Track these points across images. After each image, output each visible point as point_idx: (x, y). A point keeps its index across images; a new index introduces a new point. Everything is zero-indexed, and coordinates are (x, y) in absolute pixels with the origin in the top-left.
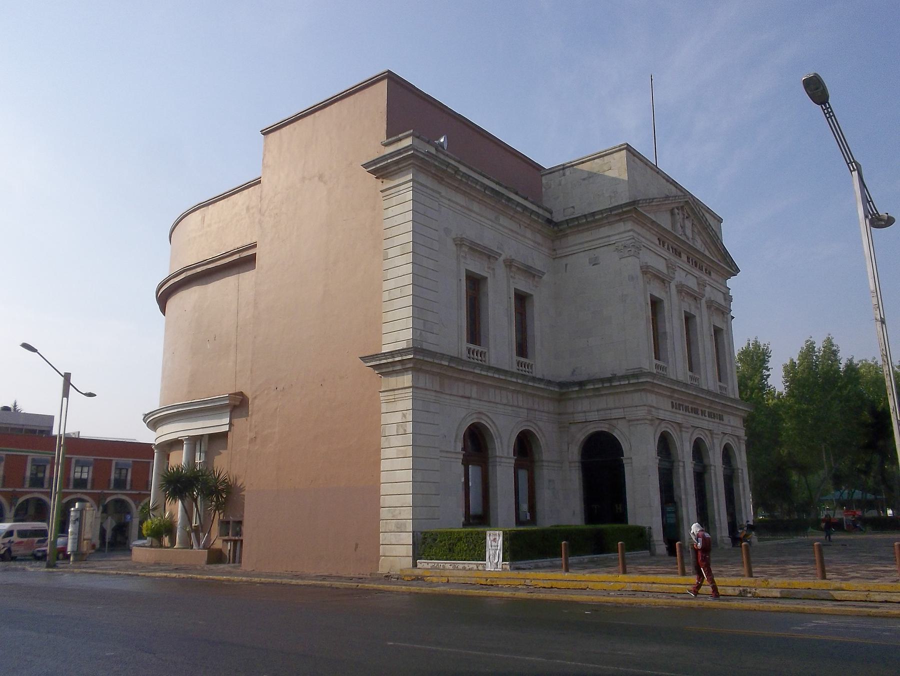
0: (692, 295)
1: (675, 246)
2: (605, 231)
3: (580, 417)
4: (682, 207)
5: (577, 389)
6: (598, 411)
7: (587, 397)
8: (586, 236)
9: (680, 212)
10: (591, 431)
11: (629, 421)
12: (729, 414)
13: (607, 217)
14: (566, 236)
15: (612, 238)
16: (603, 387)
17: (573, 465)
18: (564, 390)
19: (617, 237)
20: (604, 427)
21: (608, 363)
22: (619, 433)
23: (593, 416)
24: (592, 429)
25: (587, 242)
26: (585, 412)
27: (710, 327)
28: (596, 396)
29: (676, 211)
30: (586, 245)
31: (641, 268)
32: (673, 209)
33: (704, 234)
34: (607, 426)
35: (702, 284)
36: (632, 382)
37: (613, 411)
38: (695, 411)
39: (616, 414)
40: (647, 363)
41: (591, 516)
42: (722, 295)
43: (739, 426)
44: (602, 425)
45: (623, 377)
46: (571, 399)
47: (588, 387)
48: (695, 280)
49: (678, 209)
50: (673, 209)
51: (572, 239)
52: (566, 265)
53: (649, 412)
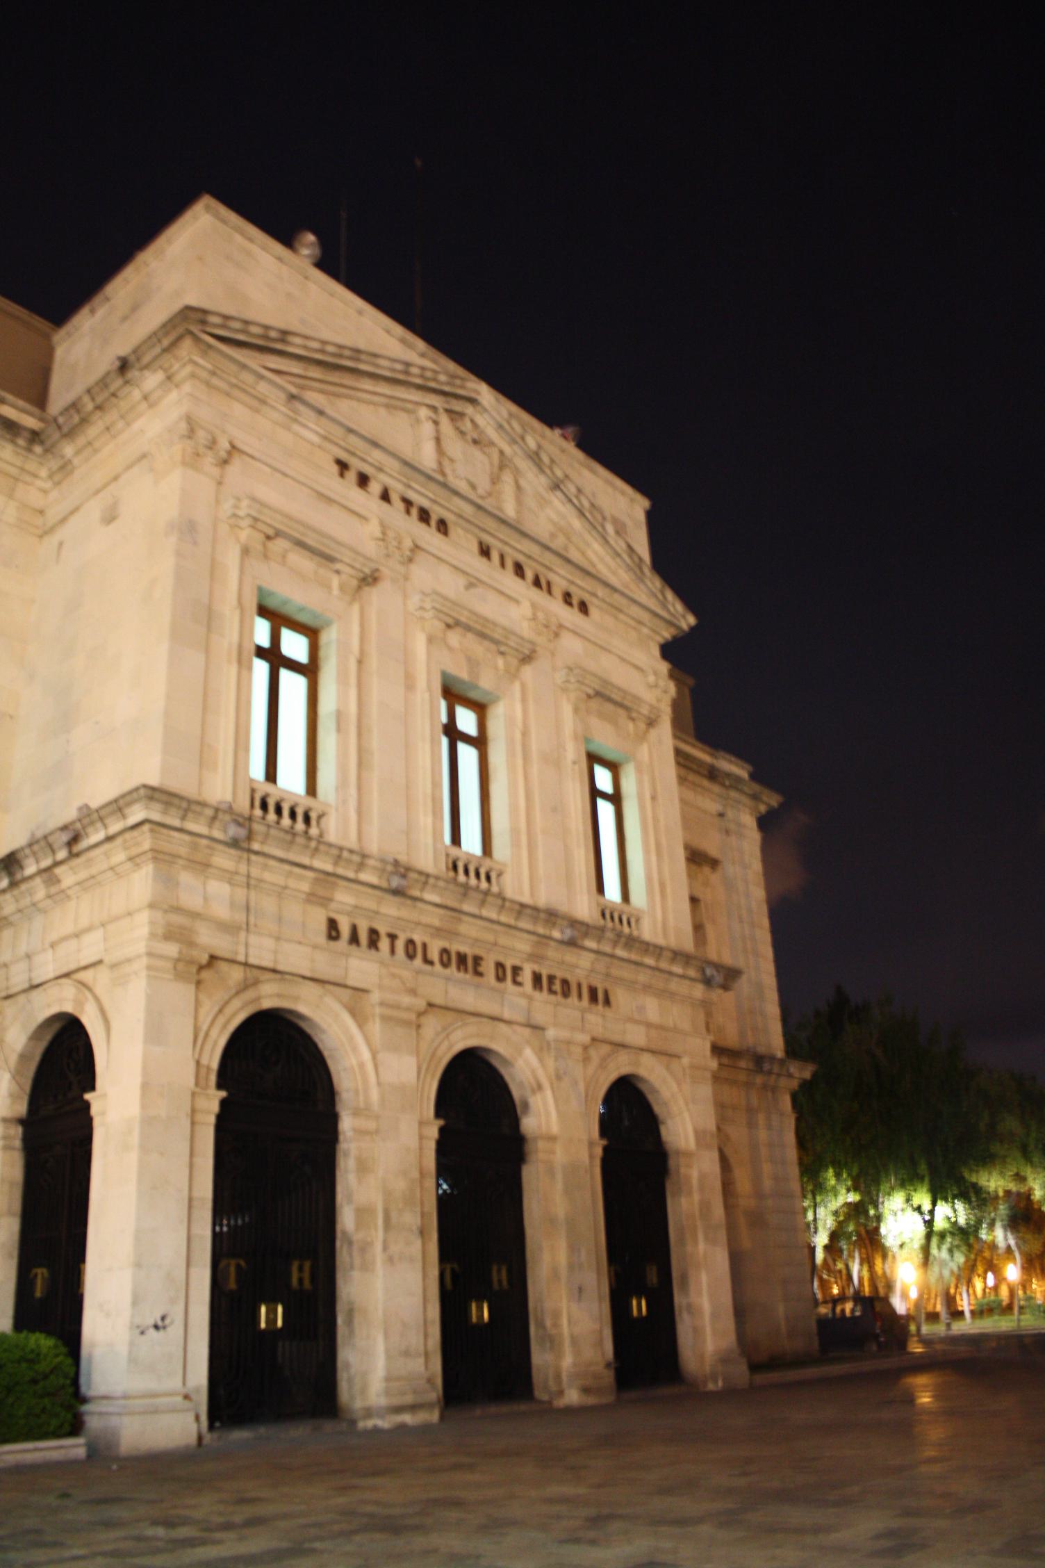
11: (114, 966)
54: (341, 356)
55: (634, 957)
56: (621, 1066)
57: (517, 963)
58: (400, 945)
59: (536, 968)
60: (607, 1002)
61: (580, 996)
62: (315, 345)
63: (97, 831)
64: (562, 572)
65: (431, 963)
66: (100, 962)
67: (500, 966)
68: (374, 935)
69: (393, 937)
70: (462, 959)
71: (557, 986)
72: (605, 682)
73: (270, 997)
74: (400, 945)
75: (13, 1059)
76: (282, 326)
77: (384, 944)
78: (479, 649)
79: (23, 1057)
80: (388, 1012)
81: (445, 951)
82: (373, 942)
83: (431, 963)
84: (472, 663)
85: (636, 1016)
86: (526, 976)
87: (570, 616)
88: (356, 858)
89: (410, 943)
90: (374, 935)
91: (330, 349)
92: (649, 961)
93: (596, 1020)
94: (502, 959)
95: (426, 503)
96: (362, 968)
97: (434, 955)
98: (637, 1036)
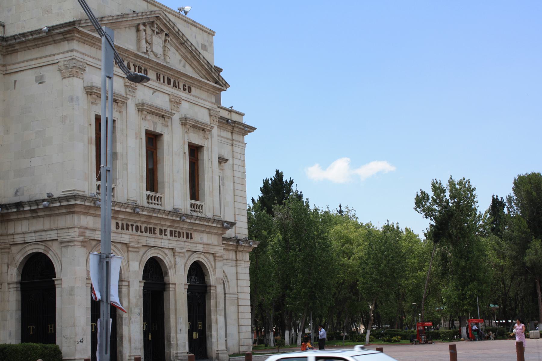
0: (157, 115)
1: (138, 64)
2: (50, 49)
3: (19, 239)
4: (153, 23)
5: (15, 210)
6: (35, 232)
7: (26, 218)
8: (35, 53)
9: (148, 28)
10: (29, 252)
11: (62, 243)
12: (199, 231)
13: (165, 11)
14: (16, 51)
15: (56, 57)
16: (38, 209)
17: (11, 286)
18: (5, 211)
19: (61, 56)
20: (40, 249)
21: (49, 183)
22: (53, 255)
23: (31, 238)
24: (30, 250)
25: (33, 60)
26: (23, 233)
27: (184, 143)
28: (34, 217)
29: (142, 27)
30: (33, 62)
31: (85, 88)
32: (139, 25)
33: (183, 49)
34: (43, 247)
35: (176, 102)
36: (62, 204)
37: (48, 233)
38: (152, 231)
39: (51, 235)
40: (84, 183)
41: (25, 336)
42: (206, 112)
43: (216, 243)
44: (40, 247)
45: (59, 199)
46: (12, 220)
47: (26, 209)
48: (167, 97)
49: (144, 24)
50: (139, 25)
51: (21, 56)
52: (15, 81)
53: (81, 234)
54: (118, 19)
55: (201, 223)
56: (195, 258)
57: (166, 228)
58: (134, 227)
59: (171, 229)
60: (191, 238)
61: (183, 237)
62: (111, 18)
63: (56, 203)
64: (183, 78)
65: (142, 232)
66: (57, 240)
67: (161, 230)
68: (128, 225)
69: (132, 226)
71: (177, 235)
72: (197, 122)
74: (134, 227)
75: (18, 264)
76: (101, 16)
77: (130, 228)
78: (156, 119)
79: (21, 263)
80: (178, 279)
81: (146, 228)
83: (142, 232)
84: (154, 124)
85: (200, 242)
86: (168, 233)
87: (183, 95)
88: (126, 205)
89: (137, 227)
90: (128, 225)
91: (114, 18)
92: (206, 223)
94: (161, 228)
95: (140, 65)
97: (143, 229)
98: (200, 248)
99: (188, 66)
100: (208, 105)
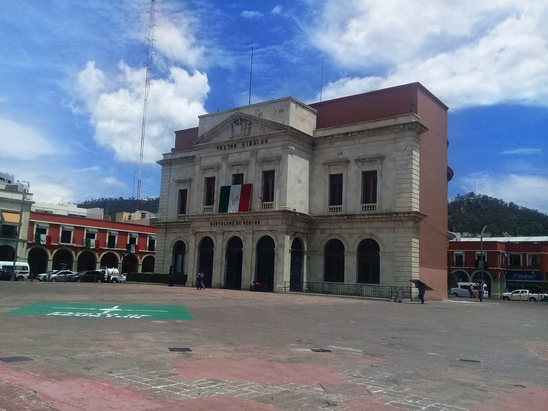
60: (259, 223)
70: (230, 223)
73: (204, 235)
82: (217, 224)
93: (255, 228)
96: (215, 229)
97: (226, 224)
99: (267, 129)
100: (280, 144)
